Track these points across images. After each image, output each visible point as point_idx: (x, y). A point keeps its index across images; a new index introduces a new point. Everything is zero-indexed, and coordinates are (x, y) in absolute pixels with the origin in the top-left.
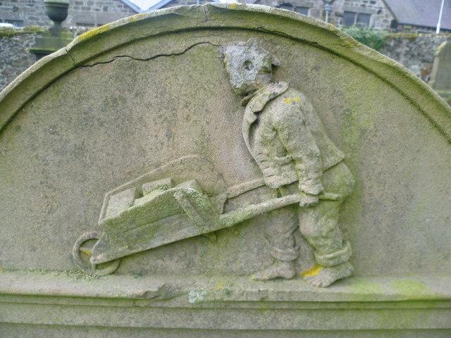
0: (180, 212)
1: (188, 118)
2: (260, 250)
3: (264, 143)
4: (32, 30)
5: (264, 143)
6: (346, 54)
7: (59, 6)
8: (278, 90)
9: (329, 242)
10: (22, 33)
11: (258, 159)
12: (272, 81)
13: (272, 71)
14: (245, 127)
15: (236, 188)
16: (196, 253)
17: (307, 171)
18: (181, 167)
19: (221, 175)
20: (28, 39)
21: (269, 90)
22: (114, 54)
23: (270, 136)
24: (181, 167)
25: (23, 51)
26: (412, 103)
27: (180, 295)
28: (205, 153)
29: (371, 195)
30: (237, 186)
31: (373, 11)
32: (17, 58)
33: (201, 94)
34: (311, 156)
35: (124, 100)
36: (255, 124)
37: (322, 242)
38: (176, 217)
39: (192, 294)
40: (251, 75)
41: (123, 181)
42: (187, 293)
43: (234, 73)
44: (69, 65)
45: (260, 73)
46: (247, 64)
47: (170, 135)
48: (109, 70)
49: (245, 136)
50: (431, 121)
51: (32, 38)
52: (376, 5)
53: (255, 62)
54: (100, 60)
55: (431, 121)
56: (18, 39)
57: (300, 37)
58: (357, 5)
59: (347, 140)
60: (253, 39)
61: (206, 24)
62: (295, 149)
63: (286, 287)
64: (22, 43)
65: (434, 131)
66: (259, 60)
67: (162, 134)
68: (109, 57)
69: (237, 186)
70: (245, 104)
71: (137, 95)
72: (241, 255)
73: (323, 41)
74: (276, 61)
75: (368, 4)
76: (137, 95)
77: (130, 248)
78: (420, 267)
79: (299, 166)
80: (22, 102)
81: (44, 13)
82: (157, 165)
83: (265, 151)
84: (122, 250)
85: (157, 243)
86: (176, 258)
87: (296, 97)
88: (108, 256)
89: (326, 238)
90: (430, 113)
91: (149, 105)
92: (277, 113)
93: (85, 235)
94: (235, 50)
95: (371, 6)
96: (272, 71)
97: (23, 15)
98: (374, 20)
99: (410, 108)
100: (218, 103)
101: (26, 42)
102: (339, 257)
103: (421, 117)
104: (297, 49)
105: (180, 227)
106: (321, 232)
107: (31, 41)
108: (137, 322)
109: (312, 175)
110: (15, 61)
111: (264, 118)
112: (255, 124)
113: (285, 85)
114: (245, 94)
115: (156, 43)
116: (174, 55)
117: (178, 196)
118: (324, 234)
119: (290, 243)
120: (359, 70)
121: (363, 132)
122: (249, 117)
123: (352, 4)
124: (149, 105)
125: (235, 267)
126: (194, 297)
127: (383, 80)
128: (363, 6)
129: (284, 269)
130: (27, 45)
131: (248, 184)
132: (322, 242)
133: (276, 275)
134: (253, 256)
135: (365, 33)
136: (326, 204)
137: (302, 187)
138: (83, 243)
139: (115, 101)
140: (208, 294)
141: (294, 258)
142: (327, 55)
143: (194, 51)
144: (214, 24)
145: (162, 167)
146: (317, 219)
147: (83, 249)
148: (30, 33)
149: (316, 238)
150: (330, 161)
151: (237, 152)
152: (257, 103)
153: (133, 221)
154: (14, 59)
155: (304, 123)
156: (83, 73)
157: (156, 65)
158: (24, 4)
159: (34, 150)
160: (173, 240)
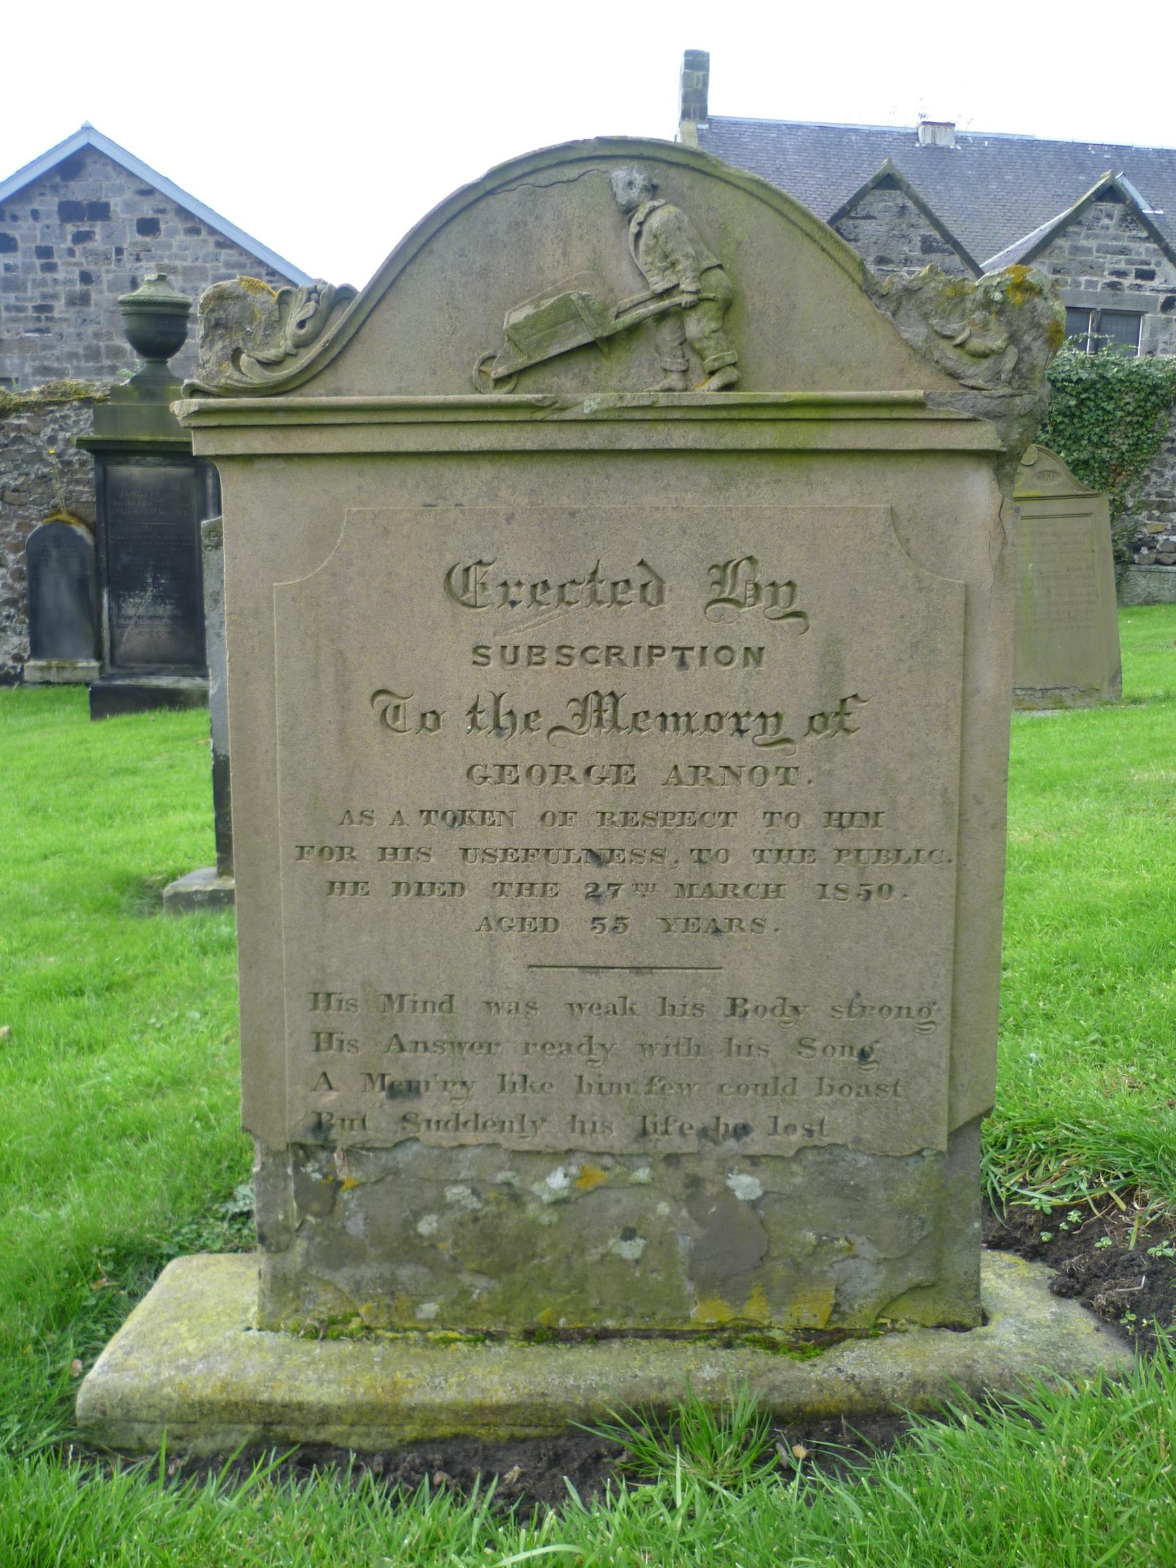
0: (576, 316)
1: (581, 238)
2: (651, 365)
3: (647, 253)
4: (65, 394)
5: (647, 253)
6: (714, 172)
7: (162, 310)
8: (656, 203)
9: (712, 343)
10: (37, 404)
11: (644, 269)
12: (652, 199)
13: (652, 190)
14: (631, 238)
15: (626, 302)
16: (589, 369)
17: (685, 271)
18: (576, 282)
19: (612, 290)
20: (54, 421)
21: (649, 204)
22: (519, 183)
23: (652, 242)
24: (576, 282)
25: (38, 457)
26: (781, 213)
27: (576, 404)
28: (597, 267)
29: (753, 304)
30: (626, 300)
31: (1150, 302)
32: (22, 479)
33: (593, 214)
34: (687, 256)
35: (525, 223)
36: (638, 235)
37: (706, 343)
38: (571, 322)
39: (586, 403)
40: (634, 193)
41: (523, 298)
42: (582, 403)
43: (620, 192)
44: (481, 192)
45: (641, 191)
46: (630, 184)
47: (565, 254)
48: (513, 197)
49: (632, 248)
50: (801, 229)
51: (64, 417)
52: (1156, 283)
53: (637, 183)
54: (506, 188)
55: (801, 229)
56: (24, 421)
57: (675, 160)
58: (1090, 284)
59: (725, 251)
60: (635, 164)
61: (595, 154)
62: (673, 251)
63: (675, 399)
64: (37, 434)
65: (806, 241)
66: (639, 179)
67: (558, 254)
68: (514, 185)
69: (626, 300)
70: (629, 222)
71: (536, 218)
72: (633, 371)
73: (693, 162)
74: (655, 181)
75: (1130, 280)
76: (536, 218)
77: (530, 357)
78: (814, 382)
79: (679, 267)
80: (438, 226)
81: (81, 351)
82: (554, 283)
83: (650, 260)
84: (522, 361)
85: (555, 351)
86: (570, 375)
87: (672, 209)
88: (508, 368)
89: (708, 338)
90: (831, 252)
91: (547, 227)
92: (655, 221)
93: (486, 354)
94: (620, 174)
95: (1139, 287)
96: (652, 190)
97: (16, 361)
98: (1153, 333)
99: (779, 219)
100: (608, 221)
101: (48, 431)
102: (723, 357)
103: (791, 227)
104: (673, 172)
105: (575, 333)
106: (703, 332)
107: (62, 429)
108: (533, 443)
109: (690, 274)
110: (15, 490)
111: (646, 228)
112: (638, 235)
113: (663, 201)
114: (629, 211)
115: (553, 172)
116: (569, 181)
117: (574, 297)
118: (707, 334)
119: (679, 353)
120: (730, 187)
121: (739, 244)
122: (633, 228)
123: (1077, 284)
124: (547, 227)
125: (628, 383)
126: (590, 404)
127: (751, 194)
128: (1113, 286)
129: (674, 380)
130: (52, 440)
131: (637, 297)
132: (706, 343)
133: (667, 386)
134: (645, 372)
135: (1104, 365)
136: (707, 305)
137: (682, 287)
138: (484, 362)
139: (517, 224)
140: (602, 402)
141: (683, 368)
142: (700, 176)
143: (586, 177)
144: (602, 153)
145: (559, 284)
146: (699, 320)
147: (483, 368)
148: (60, 404)
149: (700, 340)
150: (705, 264)
151: (625, 267)
152: (639, 216)
153: (533, 327)
154: (13, 483)
155: (679, 228)
156: (491, 200)
157: (554, 191)
158: (21, 327)
159: (443, 272)
160: (569, 348)
